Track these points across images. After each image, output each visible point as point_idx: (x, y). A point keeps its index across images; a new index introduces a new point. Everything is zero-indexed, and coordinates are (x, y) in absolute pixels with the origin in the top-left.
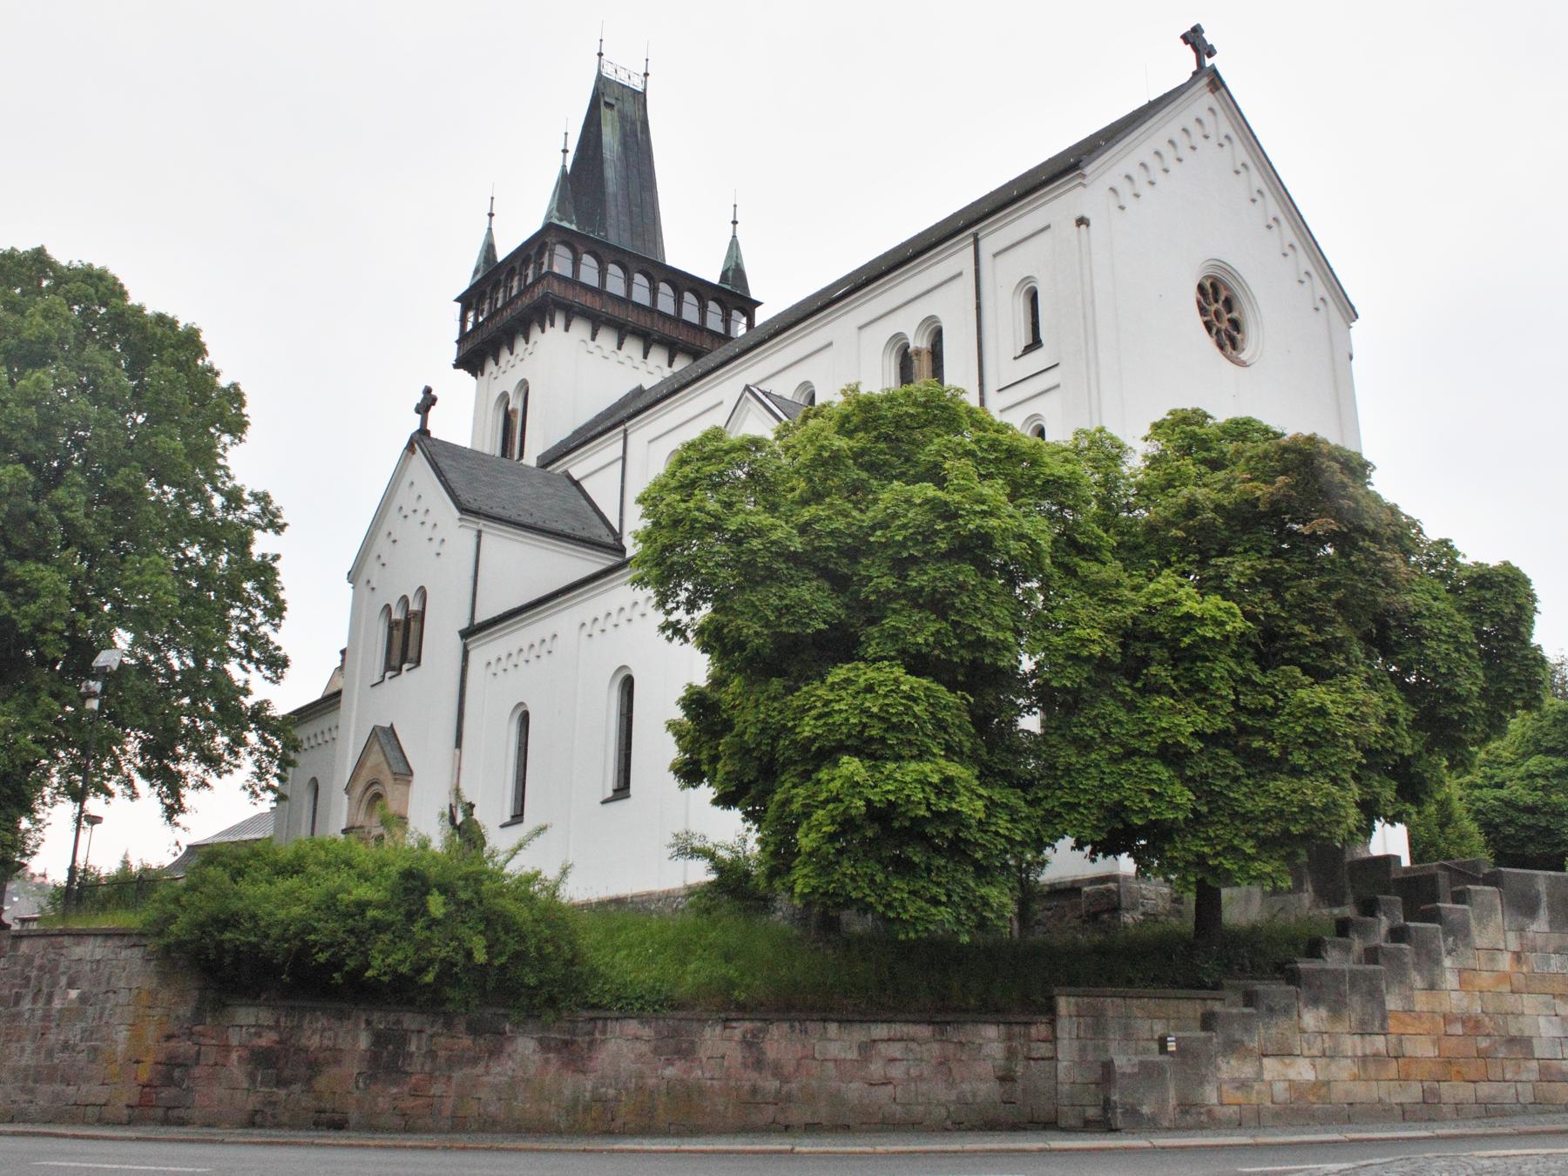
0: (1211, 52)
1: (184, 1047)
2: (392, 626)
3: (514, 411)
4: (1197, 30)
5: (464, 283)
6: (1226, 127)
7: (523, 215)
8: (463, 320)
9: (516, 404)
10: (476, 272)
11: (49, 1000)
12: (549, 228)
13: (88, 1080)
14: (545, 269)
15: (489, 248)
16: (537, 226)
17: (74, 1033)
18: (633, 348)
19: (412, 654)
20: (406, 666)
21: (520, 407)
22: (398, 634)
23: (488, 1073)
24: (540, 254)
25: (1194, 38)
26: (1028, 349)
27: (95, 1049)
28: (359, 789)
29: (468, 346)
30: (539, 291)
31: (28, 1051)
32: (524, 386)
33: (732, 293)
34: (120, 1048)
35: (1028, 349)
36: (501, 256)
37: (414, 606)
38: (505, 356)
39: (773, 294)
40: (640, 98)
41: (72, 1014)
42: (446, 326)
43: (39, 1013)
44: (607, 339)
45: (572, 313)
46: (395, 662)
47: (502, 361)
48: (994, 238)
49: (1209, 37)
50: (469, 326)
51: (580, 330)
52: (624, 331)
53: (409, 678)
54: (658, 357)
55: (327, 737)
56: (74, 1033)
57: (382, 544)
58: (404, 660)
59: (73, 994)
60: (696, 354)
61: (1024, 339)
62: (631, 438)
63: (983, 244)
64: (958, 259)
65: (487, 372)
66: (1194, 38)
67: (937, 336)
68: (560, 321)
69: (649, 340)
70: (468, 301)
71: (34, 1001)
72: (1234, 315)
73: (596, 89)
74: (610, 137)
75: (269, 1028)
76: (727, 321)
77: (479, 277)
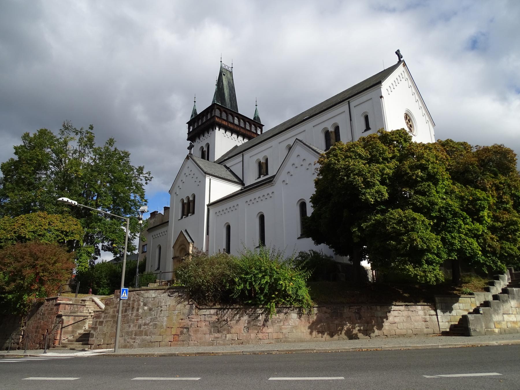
0: (402, 57)
1: (186, 322)
2: (183, 204)
3: (205, 151)
4: (398, 51)
5: (189, 120)
6: (407, 76)
7: (205, 101)
8: (189, 128)
9: (205, 149)
10: (192, 116)
11: (138, 310)
12: (213, 105)
13: (154, 334)
14: (213, 115)
15: (195, 111)
16: (210, 104)
17: (148, 320)
18: (234, 136)
19: (191, 211)
20: (189, 214)
21: (206, 150)
22: (186, 206)
23: (284, 325)
24: (212, 111)
25: (398, 53)
26: (365, 131)
27: (156, 324)
28: (177, 247)
29: (191, 135)
30: (212, 120)
31: (132, 326)
32: (208, 146)
33: (256, 123)
34: (165, 324)
35: (365, 131)
36: (198, 113)
37: (191, 199)
38: (202, 137)
39: (269, 123)
40: (231, 73)
41: (145, 314)
42: (184, 131)
43: (134, 314)
44: (229, 133)
45: (221, 126)
46: (185, 213)
47: (201, 138)
48: (354, 102)
49: (401, 53)
50: (191, 130)
51: (222, 131)
52: (233, 131)
53: (190, 217)
54: (240, 138)
55: (163, 234)
56: (148, 320)
57: (179, 183)
58: (188, 212)
59: (146, 308)
60: (250, 138)
61: (364, 128)
62: (244, 156)
63: (351, 104)
64: (344, 107)
65: (196, 141)
66: (398, 53)
67: (337, 129)
68: (217, 129)
69: (238, 134)
70: (190, 123)
71: (132, 311)
72: (411, 123)
73: (221, 70)
74: (225, 83)
75: (214, 314)
76: (256, 130)
77: (194, 117)
